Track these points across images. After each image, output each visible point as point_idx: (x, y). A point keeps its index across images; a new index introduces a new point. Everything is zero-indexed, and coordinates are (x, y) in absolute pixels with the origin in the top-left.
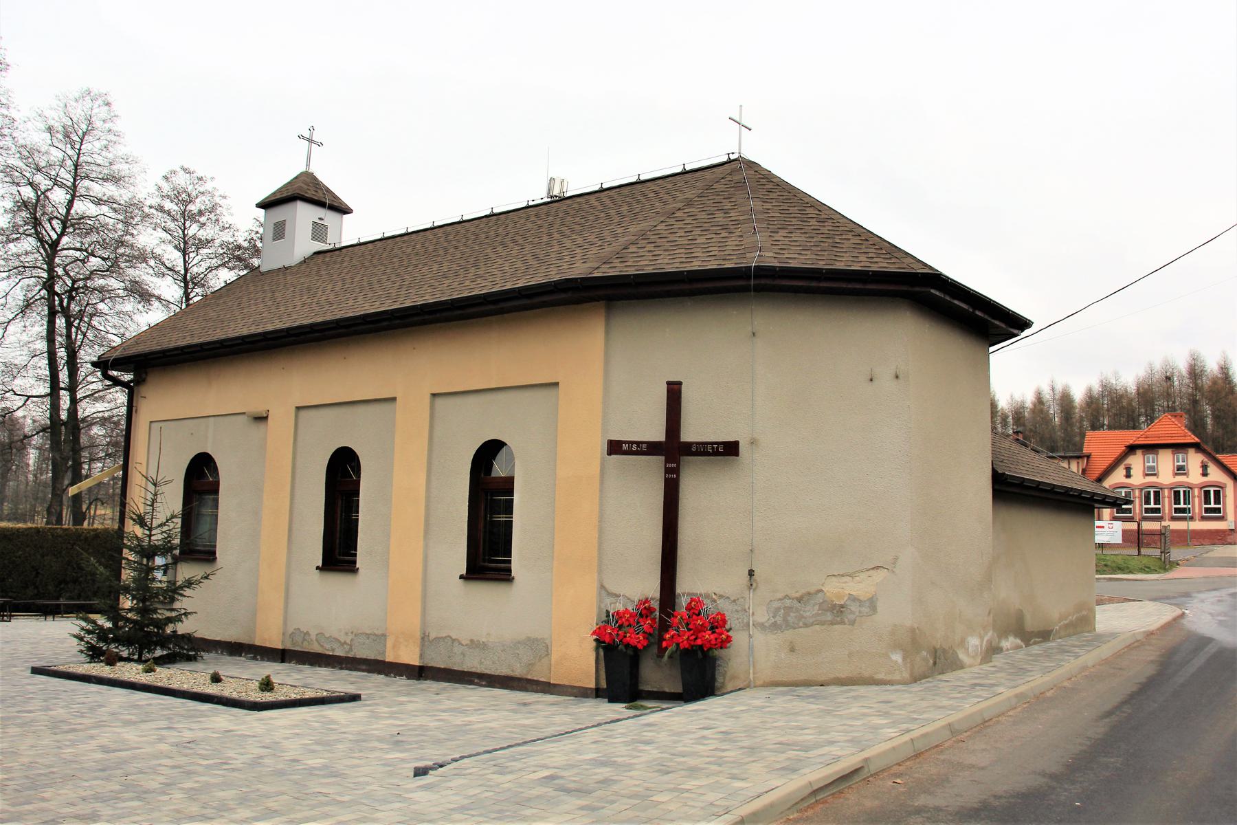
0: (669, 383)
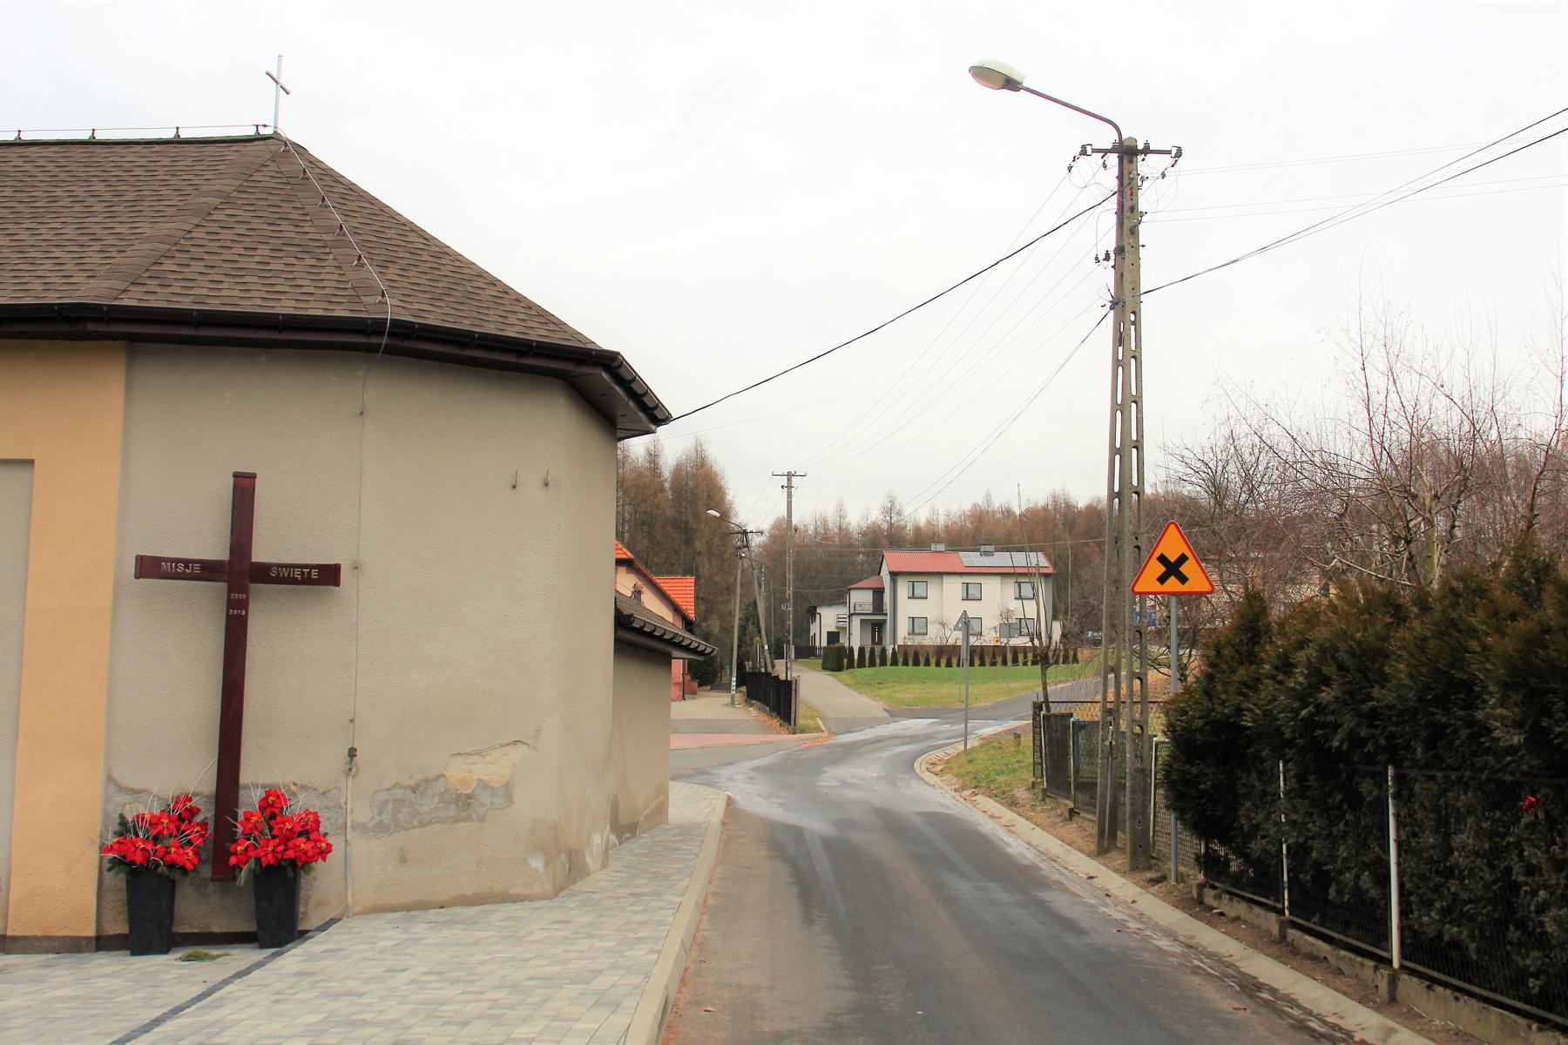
0: (236, 475)
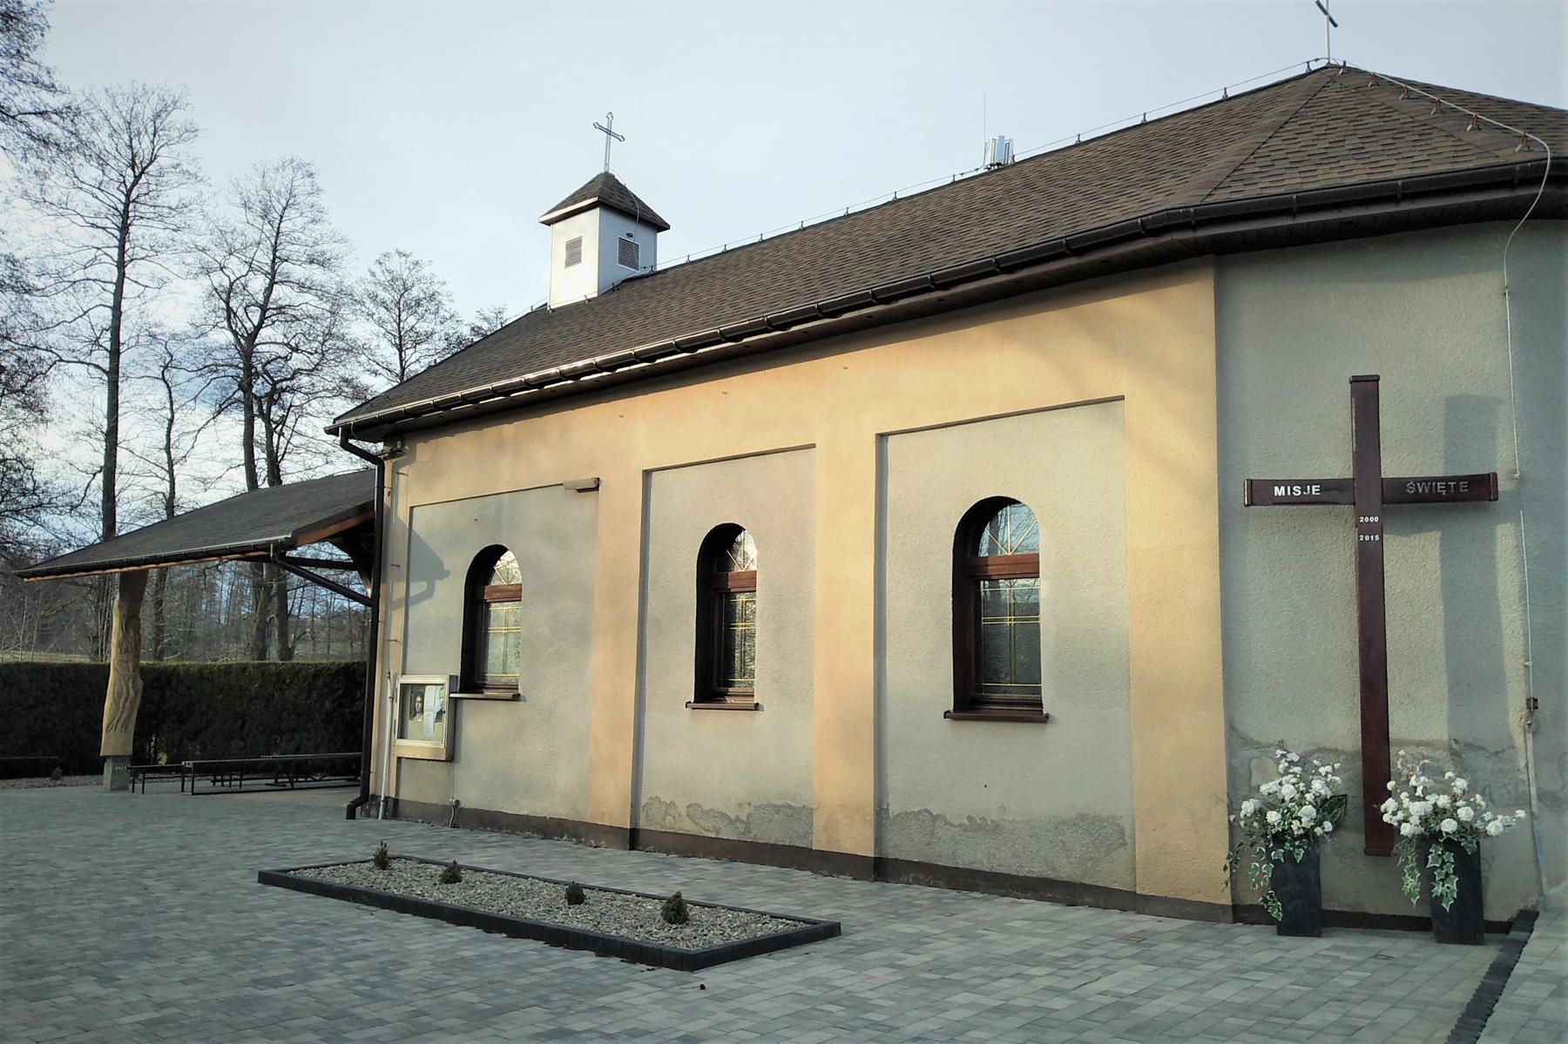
0: (1355, 380)
